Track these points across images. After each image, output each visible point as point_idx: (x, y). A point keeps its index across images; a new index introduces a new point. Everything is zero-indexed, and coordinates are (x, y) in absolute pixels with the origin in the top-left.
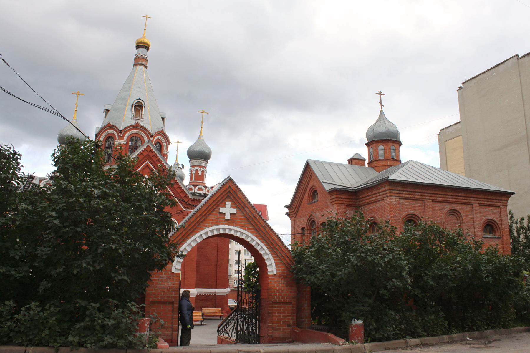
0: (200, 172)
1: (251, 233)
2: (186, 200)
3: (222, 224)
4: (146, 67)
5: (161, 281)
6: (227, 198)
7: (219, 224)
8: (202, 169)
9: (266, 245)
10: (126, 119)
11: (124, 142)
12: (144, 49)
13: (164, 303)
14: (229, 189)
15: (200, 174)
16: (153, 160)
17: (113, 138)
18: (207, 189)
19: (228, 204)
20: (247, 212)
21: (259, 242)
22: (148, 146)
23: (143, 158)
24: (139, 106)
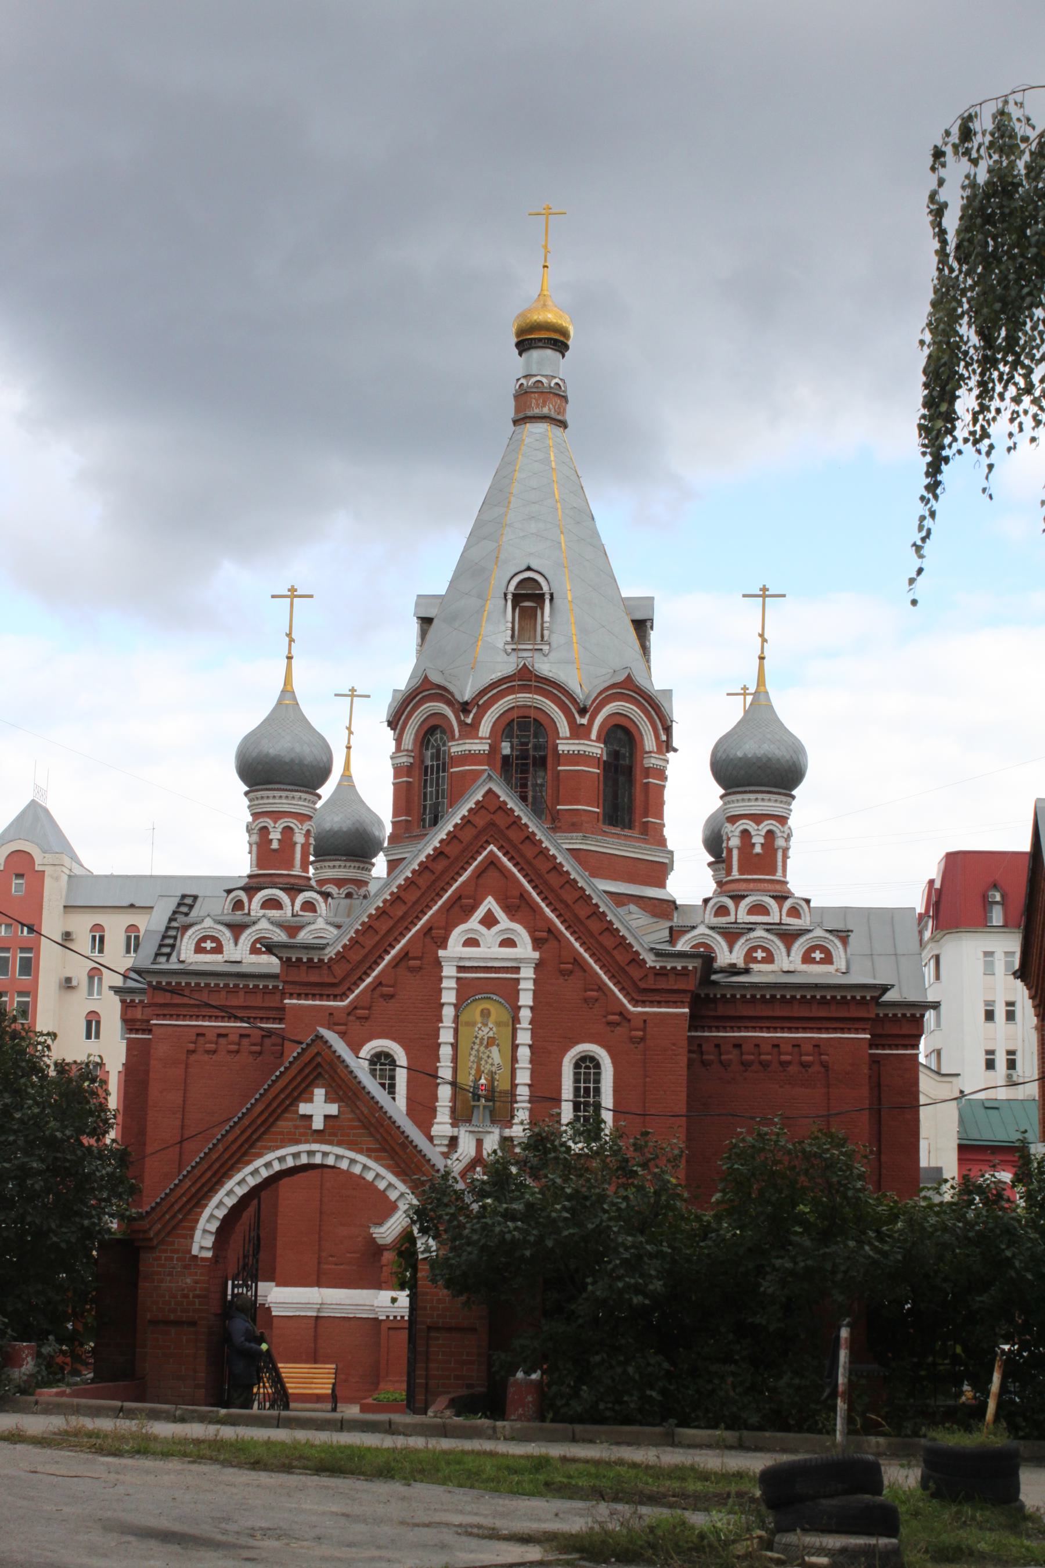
0: (758, 840)
1: (377, 1160)
2: (636, 974)
3: (307, 1142)
4: (563, 424)
5: (170, 1274)
6: (316, 1078)
7: (298, 1142)
8: (766, 826)
10: (491, 651)
11: (480, 746)
12: (549, 352)
13: (178, 1323)
14: (319, 1059)
15: (758, 849)
16: (510, 841)
17: (444, 732)
18: (788, 904)
19: (319, 1093)
20: (362, 1112)
22: (490, 791)
23: (477, 837)
24: (529, 599)
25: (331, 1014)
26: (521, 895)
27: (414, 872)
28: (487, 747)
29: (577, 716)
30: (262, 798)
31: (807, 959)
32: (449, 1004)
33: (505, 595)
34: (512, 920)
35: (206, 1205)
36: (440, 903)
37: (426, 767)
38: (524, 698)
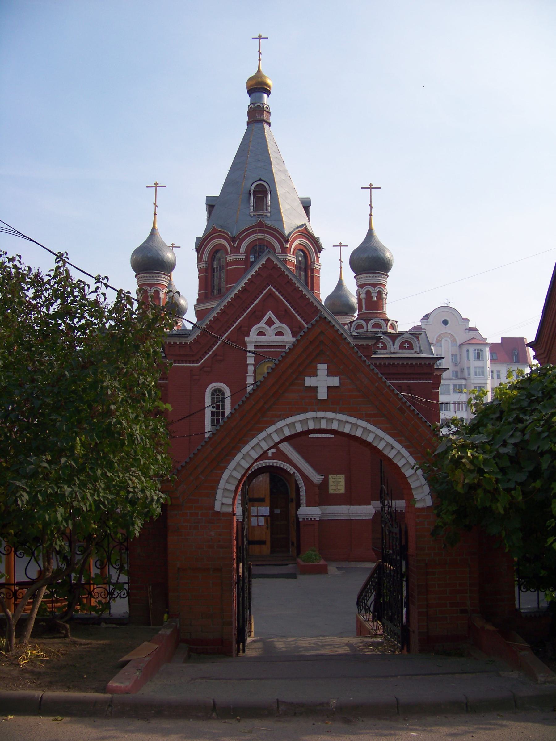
7: (305, 411)
9: (406, 447)
19: (322, 368)
21: (391, 440)
22: (269, 259)
25: (191, 370)
26: (285, 310)
27: (232, 299)
28: (244, 257)
29: (284, 243)
30: (144, 277)
31: (402, 347)
32: (251, 364)
33: (250, 191)
34: (281, 323)
35: (226, 468)
36: (245, 314)
37: (214, 268)
38: (260, 235)
